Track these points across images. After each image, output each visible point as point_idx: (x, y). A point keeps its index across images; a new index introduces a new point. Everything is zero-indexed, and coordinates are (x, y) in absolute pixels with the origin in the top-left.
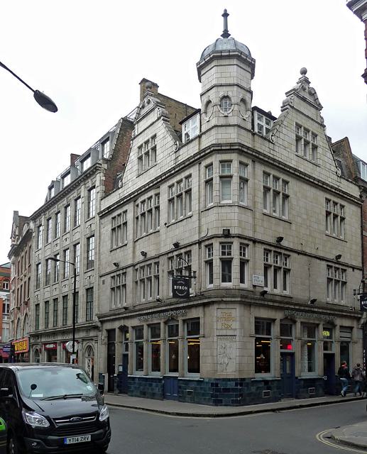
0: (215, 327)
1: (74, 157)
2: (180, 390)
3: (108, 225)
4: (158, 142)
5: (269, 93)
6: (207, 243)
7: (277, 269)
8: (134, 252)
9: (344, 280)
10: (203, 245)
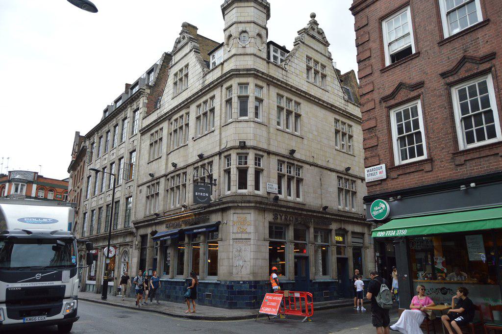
0: (231, 231)
1: (127, 85)
2: (195, 293)
3: (147, 140)
4: (191, 71)
5: (283, 30)
6: (226, 154)
7: (290, 179)
8: (167, 164)
9: (354, 190)
10: (223, 156)
